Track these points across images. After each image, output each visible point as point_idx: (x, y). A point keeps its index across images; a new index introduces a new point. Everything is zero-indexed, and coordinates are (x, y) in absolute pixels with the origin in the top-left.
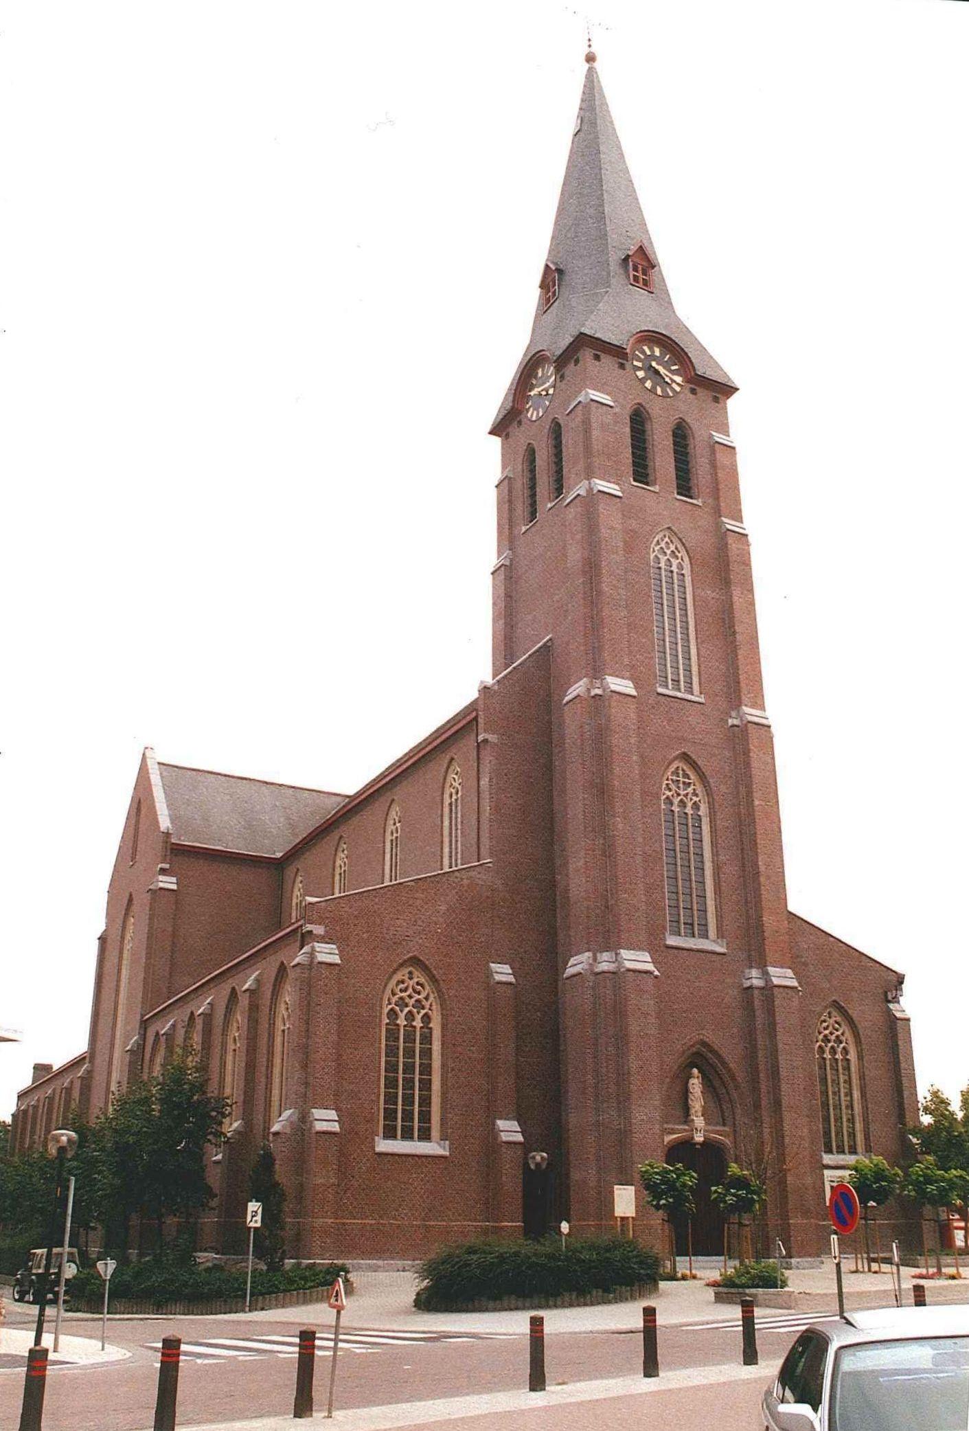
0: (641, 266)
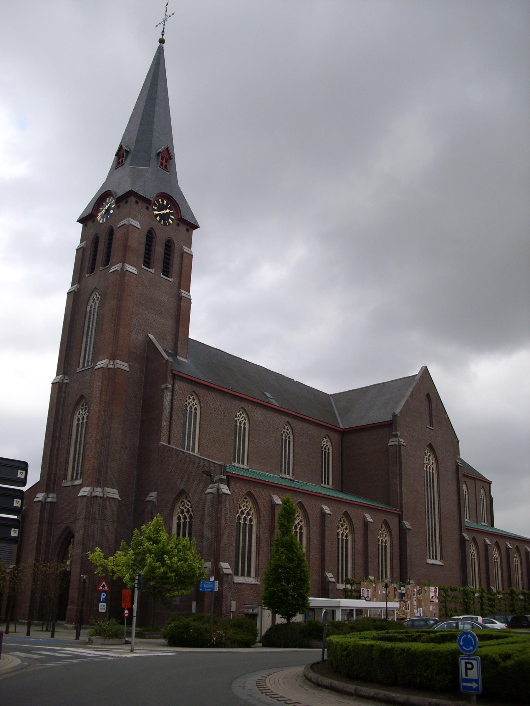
0: (166, 158)
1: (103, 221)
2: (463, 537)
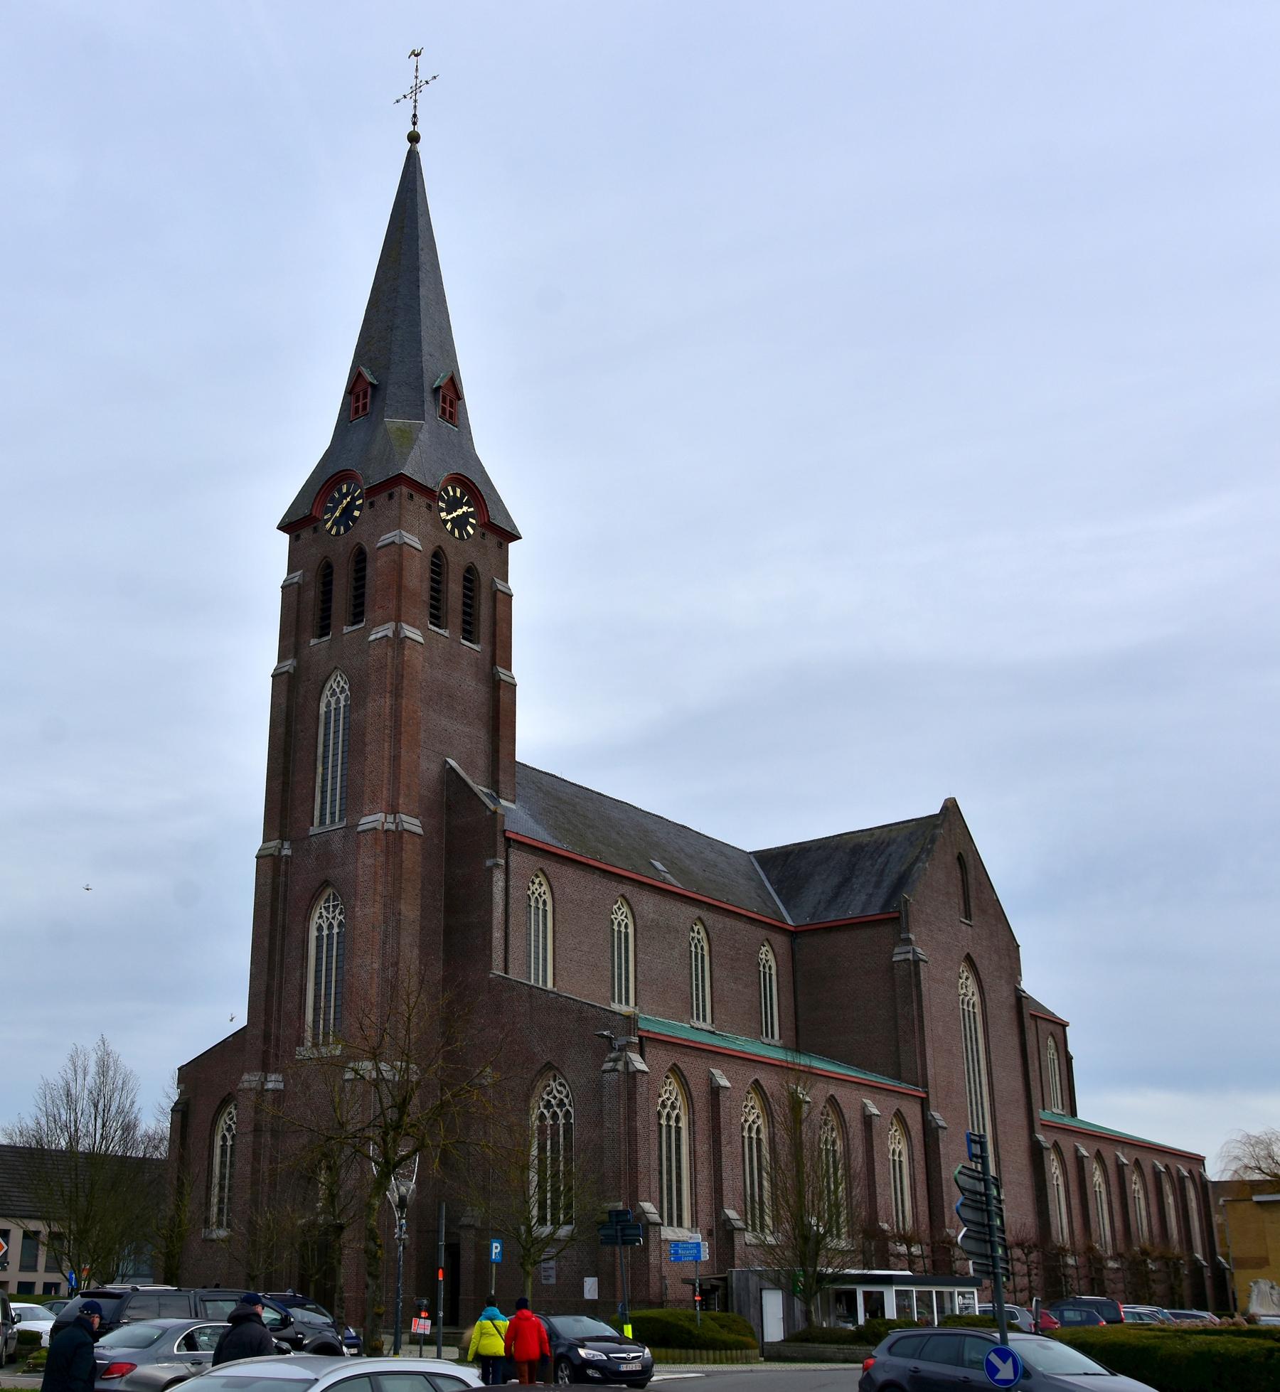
2: (1038, 1142)
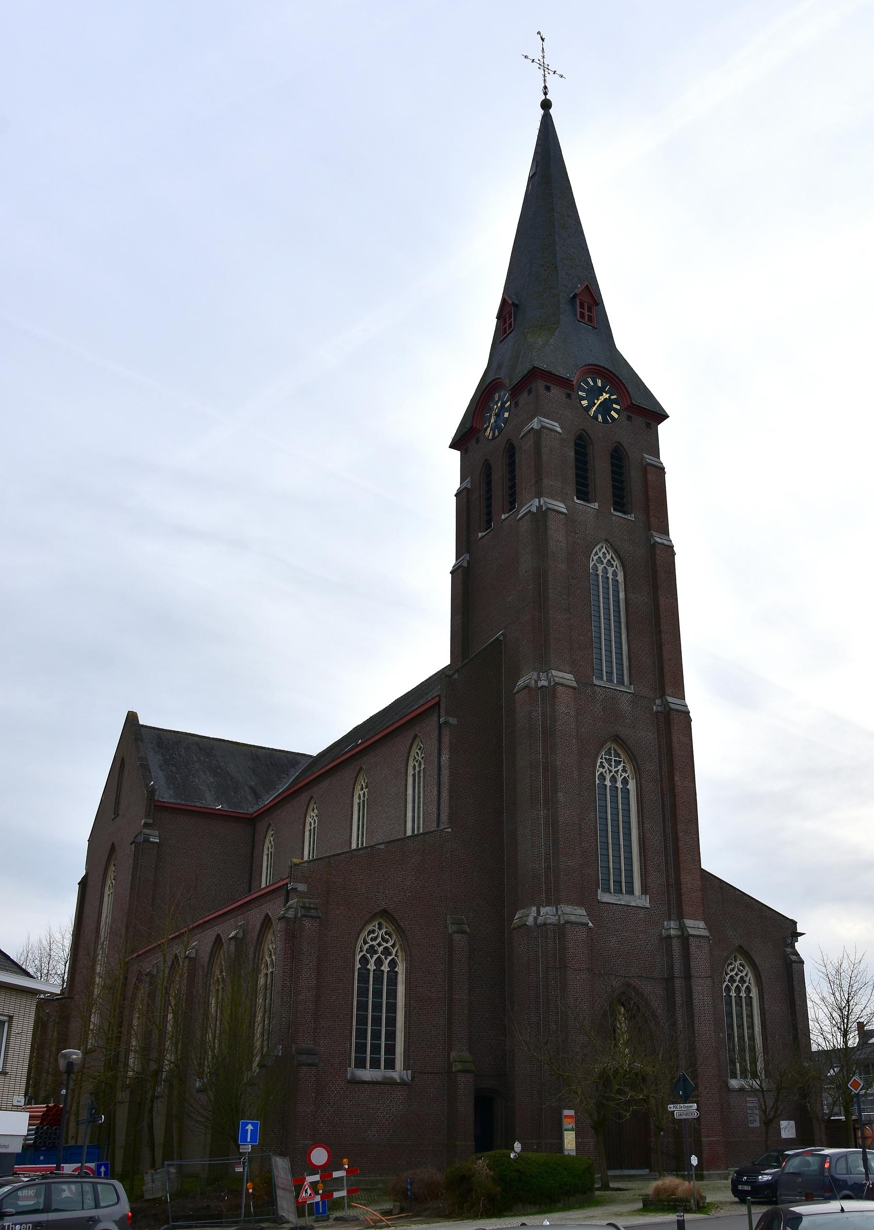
1: (494, 434)
